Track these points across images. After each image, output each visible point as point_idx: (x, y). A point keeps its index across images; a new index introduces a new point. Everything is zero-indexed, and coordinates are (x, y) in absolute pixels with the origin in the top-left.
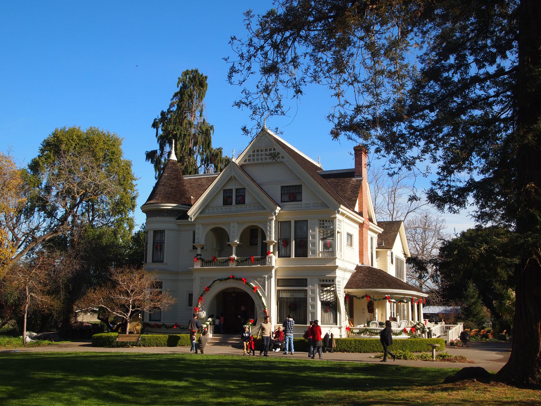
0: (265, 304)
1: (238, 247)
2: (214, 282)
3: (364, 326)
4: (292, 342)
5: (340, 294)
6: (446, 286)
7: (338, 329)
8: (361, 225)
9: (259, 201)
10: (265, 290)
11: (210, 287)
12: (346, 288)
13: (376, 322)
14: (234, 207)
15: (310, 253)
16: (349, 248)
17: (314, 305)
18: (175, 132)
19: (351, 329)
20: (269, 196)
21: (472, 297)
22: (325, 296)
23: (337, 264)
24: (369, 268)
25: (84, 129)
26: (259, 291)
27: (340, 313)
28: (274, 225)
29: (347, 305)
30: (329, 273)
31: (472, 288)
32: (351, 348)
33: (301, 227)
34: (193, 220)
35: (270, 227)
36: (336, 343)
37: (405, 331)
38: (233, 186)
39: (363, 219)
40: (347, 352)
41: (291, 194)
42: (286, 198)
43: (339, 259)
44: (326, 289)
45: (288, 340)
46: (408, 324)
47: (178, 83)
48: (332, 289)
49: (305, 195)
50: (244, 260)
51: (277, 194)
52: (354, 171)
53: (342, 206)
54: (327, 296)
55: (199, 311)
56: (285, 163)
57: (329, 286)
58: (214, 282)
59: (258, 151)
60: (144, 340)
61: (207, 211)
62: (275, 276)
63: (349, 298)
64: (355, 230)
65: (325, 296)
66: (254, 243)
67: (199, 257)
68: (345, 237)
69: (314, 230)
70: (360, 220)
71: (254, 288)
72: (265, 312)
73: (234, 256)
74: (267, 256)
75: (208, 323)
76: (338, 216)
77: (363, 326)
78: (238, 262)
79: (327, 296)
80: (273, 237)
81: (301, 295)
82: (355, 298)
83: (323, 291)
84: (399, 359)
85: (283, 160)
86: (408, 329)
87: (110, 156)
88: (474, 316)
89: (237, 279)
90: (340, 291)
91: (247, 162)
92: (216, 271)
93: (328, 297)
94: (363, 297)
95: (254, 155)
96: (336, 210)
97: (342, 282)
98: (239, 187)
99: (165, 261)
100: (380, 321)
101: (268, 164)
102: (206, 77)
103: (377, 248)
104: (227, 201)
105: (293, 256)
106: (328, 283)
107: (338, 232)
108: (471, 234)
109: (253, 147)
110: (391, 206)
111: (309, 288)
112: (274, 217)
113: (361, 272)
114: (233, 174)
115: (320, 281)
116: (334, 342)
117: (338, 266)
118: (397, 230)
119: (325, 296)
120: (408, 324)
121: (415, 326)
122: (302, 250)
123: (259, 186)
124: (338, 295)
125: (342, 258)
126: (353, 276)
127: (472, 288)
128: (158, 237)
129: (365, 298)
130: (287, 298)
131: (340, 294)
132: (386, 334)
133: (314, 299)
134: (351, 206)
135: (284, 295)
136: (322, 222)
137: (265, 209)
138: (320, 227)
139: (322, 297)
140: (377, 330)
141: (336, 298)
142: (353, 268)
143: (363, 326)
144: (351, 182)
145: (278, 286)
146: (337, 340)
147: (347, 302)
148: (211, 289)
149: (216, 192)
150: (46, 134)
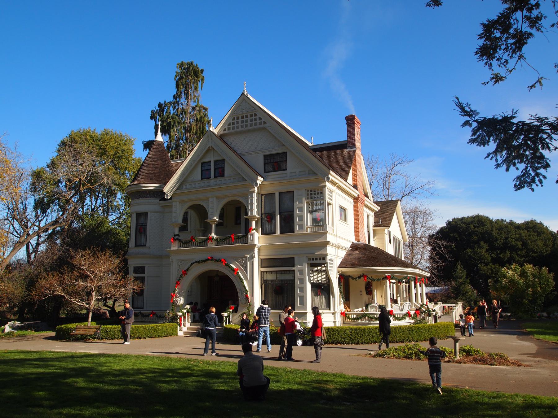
0: (247, 288)
1: (218, 225)
2: (192, 264)
3: (362, 311)
4: (269, 336)
5: (332, 274)
6: (441, 266)
7: (331, 314)
8: (356, 200)
10: (247, 273)
11: (187, 270)
12: (339, 267)
13: (376, 305)
14: (213, 181)
15: (297, 228)
16: (343, 223)
18: (169, 120)
19: (347, 314)
21: (461, 278)
23: (328, 240)
24: (365, 245)
26: (240, 274)
27: (334, 297)
28: (256, 198)
29: (342, 287)
30: (319, 250)
31: (460, 269)
32: (345, 339)
33: (287, 197)
34: (169, 197)
36: (327, 333)
37: (408, 315)
38: (211, 158)
39: (358, 193)
41: (275, 163)
42: (269, 168)
43: (330, 234)
44: (316, 269)
45: (262, 334)
46: (412, 307)
47: (176, 77)
48: (324, 269)
49: (290, 163)
50: (225, 239)
51: (259, 163)
52: (346, 143)
53: (331, 172)
54: (318, 277)
55: (176, 297)
56: (268, 128)
57: (320, 265)
58: (192, 264)
59: (238, 118)
60: (106, 331)
61: (184, 187)
62: (259, 255)
63: (344, 279)
64: (349, 205)
66: (235, 221)
67: (176, 238)
68: (337, 211)
69: (301, 202)
70: (355, 193)
71: (234, 270)
72: (247, 297)
73: (213, 235)
74: (249, 234)
75: (185, 311)
76: (327, 184)
77: (360, 309)
78: (218, 242)
79: (318, 277)
81: (288, 277)
83: (313, 271)
84: (409, 358)
85: (265, 126)
86: (412, 313)
88: (463, 294)
89: (216, 260)
90: (332, 270)
91: (227, 131)
92: (194, 252)
93: (320, 278)
94: (359, 277)
95: (233, 124)
97: (334, 260)
98: (217, 158)
99: (147, 245)
100: (379, 304)
101: (250, 131)
102: (202, 71)
103: (373, 227)
104: (205, 176)
106: (318, 262)
108: (456, 222)
109: (232, 113)
110: (386, 192)
111: (297, 268)
112: (256, 189)
113: (357, 250)
115: (309, 259)
117: (329, 242)
118: (394, 210)
120: (412, 307)
121: (420, 308)
122: (288, 225)
123: (240, 156)
124: (331, 276)
125: (335, 233)
126: (349, 254)
127: (460, 269)
128: (142, 220)
129: (362, 278)
130: (272, 281)
131: (332, 274)
132: (384, 316)
133: (302, 281)
134: (344, 177)
135: (269, 277)
136: (310, 193)
137: (246, 180)
138: (308, 198)
139: (312, 279)
141: (329, 279)
142: (348, 245)
143: (360, 309)
144: (344, 153)
145: (262, 267)
147: (342, 284)
148: (188, 273)
149: (194, 165)
150: (64, 135)
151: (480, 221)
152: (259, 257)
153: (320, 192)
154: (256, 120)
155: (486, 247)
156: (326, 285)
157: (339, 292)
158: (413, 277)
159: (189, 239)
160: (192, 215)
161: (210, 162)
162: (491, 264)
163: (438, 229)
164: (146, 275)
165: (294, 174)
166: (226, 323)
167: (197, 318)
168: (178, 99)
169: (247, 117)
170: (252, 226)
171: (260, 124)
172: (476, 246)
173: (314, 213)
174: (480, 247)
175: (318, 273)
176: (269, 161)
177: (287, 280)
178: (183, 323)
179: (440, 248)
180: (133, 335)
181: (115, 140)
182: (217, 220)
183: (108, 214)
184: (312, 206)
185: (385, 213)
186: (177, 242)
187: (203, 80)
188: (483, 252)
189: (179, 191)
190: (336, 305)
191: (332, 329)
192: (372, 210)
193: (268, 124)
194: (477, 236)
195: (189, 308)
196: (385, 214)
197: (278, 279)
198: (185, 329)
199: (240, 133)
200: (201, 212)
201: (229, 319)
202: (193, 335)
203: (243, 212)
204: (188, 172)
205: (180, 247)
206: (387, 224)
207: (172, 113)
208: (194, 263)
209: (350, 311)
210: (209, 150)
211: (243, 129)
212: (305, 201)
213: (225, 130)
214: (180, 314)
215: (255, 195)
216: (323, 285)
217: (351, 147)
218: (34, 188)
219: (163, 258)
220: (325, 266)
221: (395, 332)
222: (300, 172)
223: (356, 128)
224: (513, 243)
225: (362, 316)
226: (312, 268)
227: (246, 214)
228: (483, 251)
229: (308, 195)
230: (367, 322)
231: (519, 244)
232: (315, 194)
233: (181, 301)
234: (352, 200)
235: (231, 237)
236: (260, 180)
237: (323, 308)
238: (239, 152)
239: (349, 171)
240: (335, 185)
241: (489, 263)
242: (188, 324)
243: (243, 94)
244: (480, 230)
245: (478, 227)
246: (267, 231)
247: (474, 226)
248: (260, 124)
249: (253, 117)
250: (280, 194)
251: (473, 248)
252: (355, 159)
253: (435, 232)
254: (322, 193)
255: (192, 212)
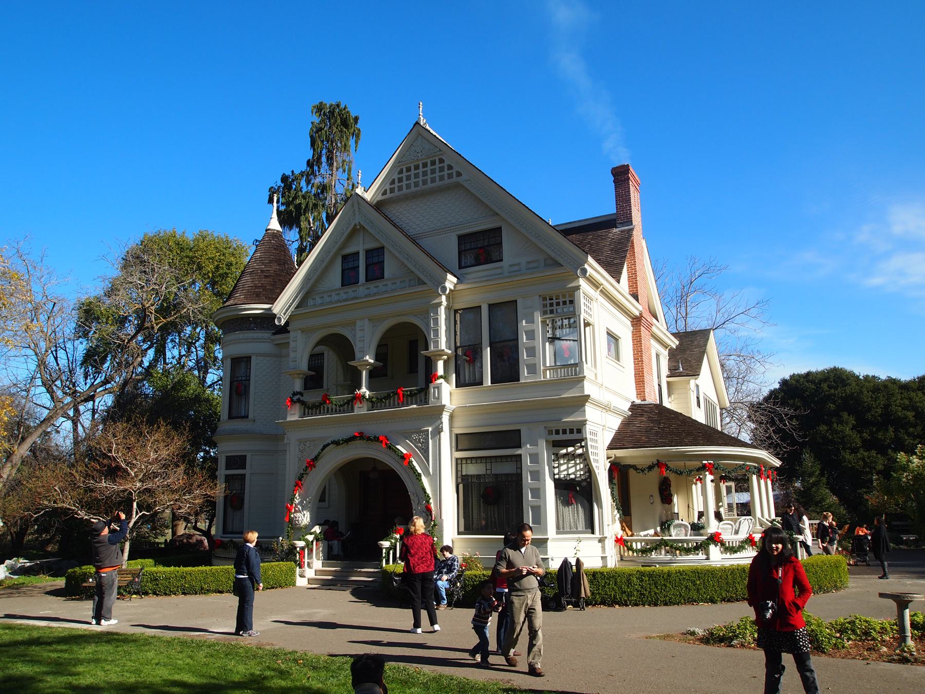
0: (429, 491)
2: (324, 447)
3: (656, 534)
5: (597, 461)
8: (637, 321)
9: (413, 269)
10: (428, 461)
11: (316, 458)
12: (610, 447)
14: (362, 288)
15: (524, 372)
17: (538, 489)
18: (298, 201)
19: (627, 541)
20: (432, 258)
21: (811, 475)
22: (565, 467)
23: (586, 393)
25: (190, 235)
26: (415, 463)
27: (600, 506)
30: (568, 416)
31: (808, 459)
32: (630, 595)
33: (505, 313)
34: (283, 322)
35: (436, 321)
36: (591, 582)
37: (750, 541)
40: (620, 604)
41: (479, 249)
42: (469, 259)
43: (591, 381)
44: (564, 451)
46: (755, 525)
48: (580, 451)
50: (385, 398)
51: (450, 249)
53: (590, 259)
54: (568, 468)
55: (296, 512)
56: (465, 184)
57: (572, 443)
58: (324, 447)
59: (409, 170)
61: (311, 302)
62: (451, 427)
63: (618, 471)
64: (624, 330)
65: (563, 467)
66: (405, 365)
67: (295, 398)
68: (602, 340)
69: (531, 321)
70: (636, 308)
71: (403, 457)
72: (429, 510)
73: (364, 391)
74: (432, 386)
75: (310, 538)
76: (582, 282)
77: (652, 532)
79: (568, 468)
80: (442, 341)
81: (508, 468)
82: (631, 471)
83: (558, 457)
85: (460, 179)
86: (757, 537)
87: (225, 270)
89: (369, 439)
91: (388, 195)
92: (331, 426)
93: (572, 470)
94: (650, 468)
95: (400, 180)
96: (578, 268)
97: (600, 434)
98: (372, 245)
99: (251, 416)
102: (356, 119)
104: (349, 278)
105: (488, 381)
107: (587, 324)
108: (797, 381)
111: (525, 451)
112: (444, 298)
113: (642, 415)
114: (358, 219)
115: (550, 432)
116: (585, 582)
119: (565, 467)
120: (755, 525)
122: (507, 372)
123: (414, 241)
124: (594, 465)
125: (599, 381)
127: (808, 459)
130: (478, 476)
131: (597, 461)
133: (537, 476)
135: (472, 470)
138: (545, 313)
139: (556, 471)
140: (687, 541)
141: (589, 471)
142: (626, 406)
143: (652, 532)
145: (457, 450)
146: (594, 575)
147: (615, 481)
148: (318, 464)
150: (132, 239)
151: (839, 378)
152: (451, 431)
153: (567, 300)
154: (441, 169)
155: (852, 421)
156: (584, 484)
157: (610, 497)
158: (755, 467)
159: (320, 399)
160: (331, 360)
161: (358, 253)
162: (861, 451)
163: (766, 392)
164: (247, 472)
165: (514, 268)
166: (388, 562)
167: (336, 551)
168: (316, 168)
169: (429, 167)
170: (436, 370)
171: (450, 176)
172: (834, 420)
173: (557, 342)
174: (841, 422)
175: (569, 460)
176: (468, 246)
177: (507, 475)
178: (306, 560)
179: (781, 420)
180: (206, 587)
181: (216, 248)
182: (372, 361)
183: (206, 372)
184: (554, 329)
185: (688, 352)
186: (298, 405)
187: (358, 136)
188: (848, 431)
189: (301, 311)
190: (605, 524)
191: (602, 573)
192: (665, 346)
193: (465, 176)
194: (834, 403)
195: (318, 531)
196: (687, 354)
197: (489, 472)
198: (310, 573)
199: (415, 196)
200: (342, 346)
201: (395, 554)
202: (326, 585)
203: (421, 344)
204: (318, 273)
205: (304, 415)
206: (694, 372)
207: (304, 190)
208: (328, 445)
209: (632, 535)
210: (356, 231)
211: (418, 188)
212: (538, 318)
213: (385, 193)
214: (300, 544)
215: (442, 311)
216: (579, 483)
217: (623, 224)
218: (82, 332)
219: (275, 438)
220: (582, 447)
221: (734, 578)
222: (529, 263)
223: (632, 189)
224: (900, 414)
225: (657, 546)
226: (555, 450)
227: (427, 348)
228: (847, 427)
229: (545, 306)
230: (669, 557)
231: (910, 414)
232: (558, 304)
233: (304, 518)
234: (628, 322)
235: (397, 393)
236: (451, 281)
237: (580, 529)
238: (412, 232)
239: (622, 265)
240: (598, 288)
241: (858, 449)
242: (318, 564)
243: (417, 123)
244: (839, 392)
245: (836, 388)
246: (467, 379)
247: (829, 386)
248: (450, 176)
249: (437, 166)
250: (491, 306)
251: (829, 424)
252: (633, 246)
253: (761, 398)
254: (572, 302)
255: (331, 353)
